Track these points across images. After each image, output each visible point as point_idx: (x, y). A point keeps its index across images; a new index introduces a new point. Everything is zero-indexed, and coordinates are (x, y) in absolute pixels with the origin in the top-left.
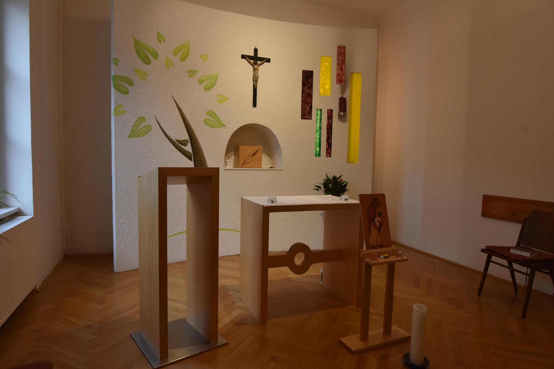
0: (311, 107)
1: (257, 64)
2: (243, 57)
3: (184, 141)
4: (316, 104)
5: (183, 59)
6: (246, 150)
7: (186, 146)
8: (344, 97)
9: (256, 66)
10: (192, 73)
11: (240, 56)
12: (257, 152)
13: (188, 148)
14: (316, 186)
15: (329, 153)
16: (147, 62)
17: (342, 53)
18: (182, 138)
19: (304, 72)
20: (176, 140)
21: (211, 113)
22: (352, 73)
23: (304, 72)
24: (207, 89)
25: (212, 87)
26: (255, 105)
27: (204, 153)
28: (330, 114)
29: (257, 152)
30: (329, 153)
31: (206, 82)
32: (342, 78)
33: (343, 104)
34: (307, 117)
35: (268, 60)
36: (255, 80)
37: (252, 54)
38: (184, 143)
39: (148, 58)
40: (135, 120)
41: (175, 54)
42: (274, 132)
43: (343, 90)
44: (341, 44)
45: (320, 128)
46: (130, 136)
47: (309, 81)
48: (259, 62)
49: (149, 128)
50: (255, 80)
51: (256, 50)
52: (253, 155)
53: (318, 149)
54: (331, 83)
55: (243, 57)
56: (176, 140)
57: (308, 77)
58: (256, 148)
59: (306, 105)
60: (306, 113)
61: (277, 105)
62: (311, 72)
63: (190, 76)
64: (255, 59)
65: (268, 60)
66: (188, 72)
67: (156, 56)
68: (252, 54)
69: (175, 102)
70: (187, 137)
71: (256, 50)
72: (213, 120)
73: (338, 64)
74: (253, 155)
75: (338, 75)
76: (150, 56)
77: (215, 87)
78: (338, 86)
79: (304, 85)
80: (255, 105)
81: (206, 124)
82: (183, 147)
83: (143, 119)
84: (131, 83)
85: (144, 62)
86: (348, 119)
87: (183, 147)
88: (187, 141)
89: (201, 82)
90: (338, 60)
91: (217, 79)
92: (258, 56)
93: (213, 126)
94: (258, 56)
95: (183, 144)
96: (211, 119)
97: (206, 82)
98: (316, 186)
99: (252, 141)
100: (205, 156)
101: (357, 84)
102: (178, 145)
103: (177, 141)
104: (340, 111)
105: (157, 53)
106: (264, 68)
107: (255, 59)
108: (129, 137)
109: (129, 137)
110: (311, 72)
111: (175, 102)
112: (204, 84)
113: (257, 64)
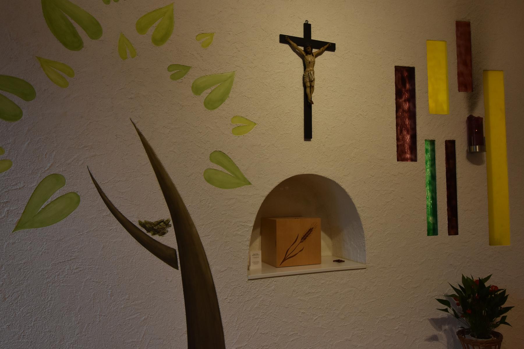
0: (414, 138)
1: (310, 53)
2: (284, 39)
3: (159, 223)
4: (424, 131)
5: (159, 41)
6: (289, 228)
7: (164, 234)
8: (476, 114)
9: (309, 58)
10: (179, 71)
11: (278, 38)
12: (311, 230)
13: (169, 239)
14: (441, 301)
15: (453, 228)
16: (76, 44)
17: (464, 32)
18: (154, 218)
19: (399, 70)
20: (141, 223)
21: (219, 157)
22: (486, 71)
23: (399, 70)
24: (211, 104)
25: (222, 100)
26: (308, 135)
27: (205, 248)
28: (450, 146)
29: (311, 230)
30: (453, 228)
31: (209, 91)
32: (468, 80)
33: (476, 130)
34: (408, 156)
35: (332, 47)
36: (308, 85)
37: (300, 34)
38: (159, 228)
39: (75, 34)
40: (35, 184)
41: (141, 29)
42: (347, 190)
43: (472, 103)
44: (462, 18)
45: (433, 177)
46: (19, 226)
47: (408, 86)
48: (314, 51)
49: (74, 200)
50: (308, 85)
51: (307, 27)
52: (304, 238)
53: (431, 218)
54: (450, 90)
55: (284, 39)
56: (141, 223)
57: (405, 80)
58: (308, 222)
59: (405, 133)
60: (406, 150)
61: (349, 134)
62: (411, 71)
63: (174, 77)
64: (307, 46)
65: (332, 47)
66: (170, 68)
67: (95, 30)
68: (300, 34)
69: (140, 134)
70: (165, 214)
71: (307, 27)
72: (226, 172)
73: (459, 55)
74: (304, 238)
75: (460, 74)
76: (80, 30)
77: (227, 102)
78: (462, 96)
79: (399, 94)
80: (308, 135)
81: (209, 180)
82: (157, 237)
83: (58, 179)
84: (28, 93)
85: (65, 44)
86: (485, 159)
87: (157, 237)
88: (168, 221)
89: (197, 90)
90: (458, 46)
91: (232, 82)
92: (313, 38)
93: (222, 185)
94: (313, 38)
95: (157, 232)
96: (220, 168)
97: (209, 91)
98: (441, 301)
99: (302, 214)
100: (208, 253)
101: (496, 90)
102: (144, 235)
103: (143, 225)
104: (470, 143)
105: (98, 24)
106: (323, 62)
107: (307, 46)
108: (17, 228)
109: (17, 228)
110: (411, 71)
111: (140, 134)
112: (205, 94)
113: (310, 53)
